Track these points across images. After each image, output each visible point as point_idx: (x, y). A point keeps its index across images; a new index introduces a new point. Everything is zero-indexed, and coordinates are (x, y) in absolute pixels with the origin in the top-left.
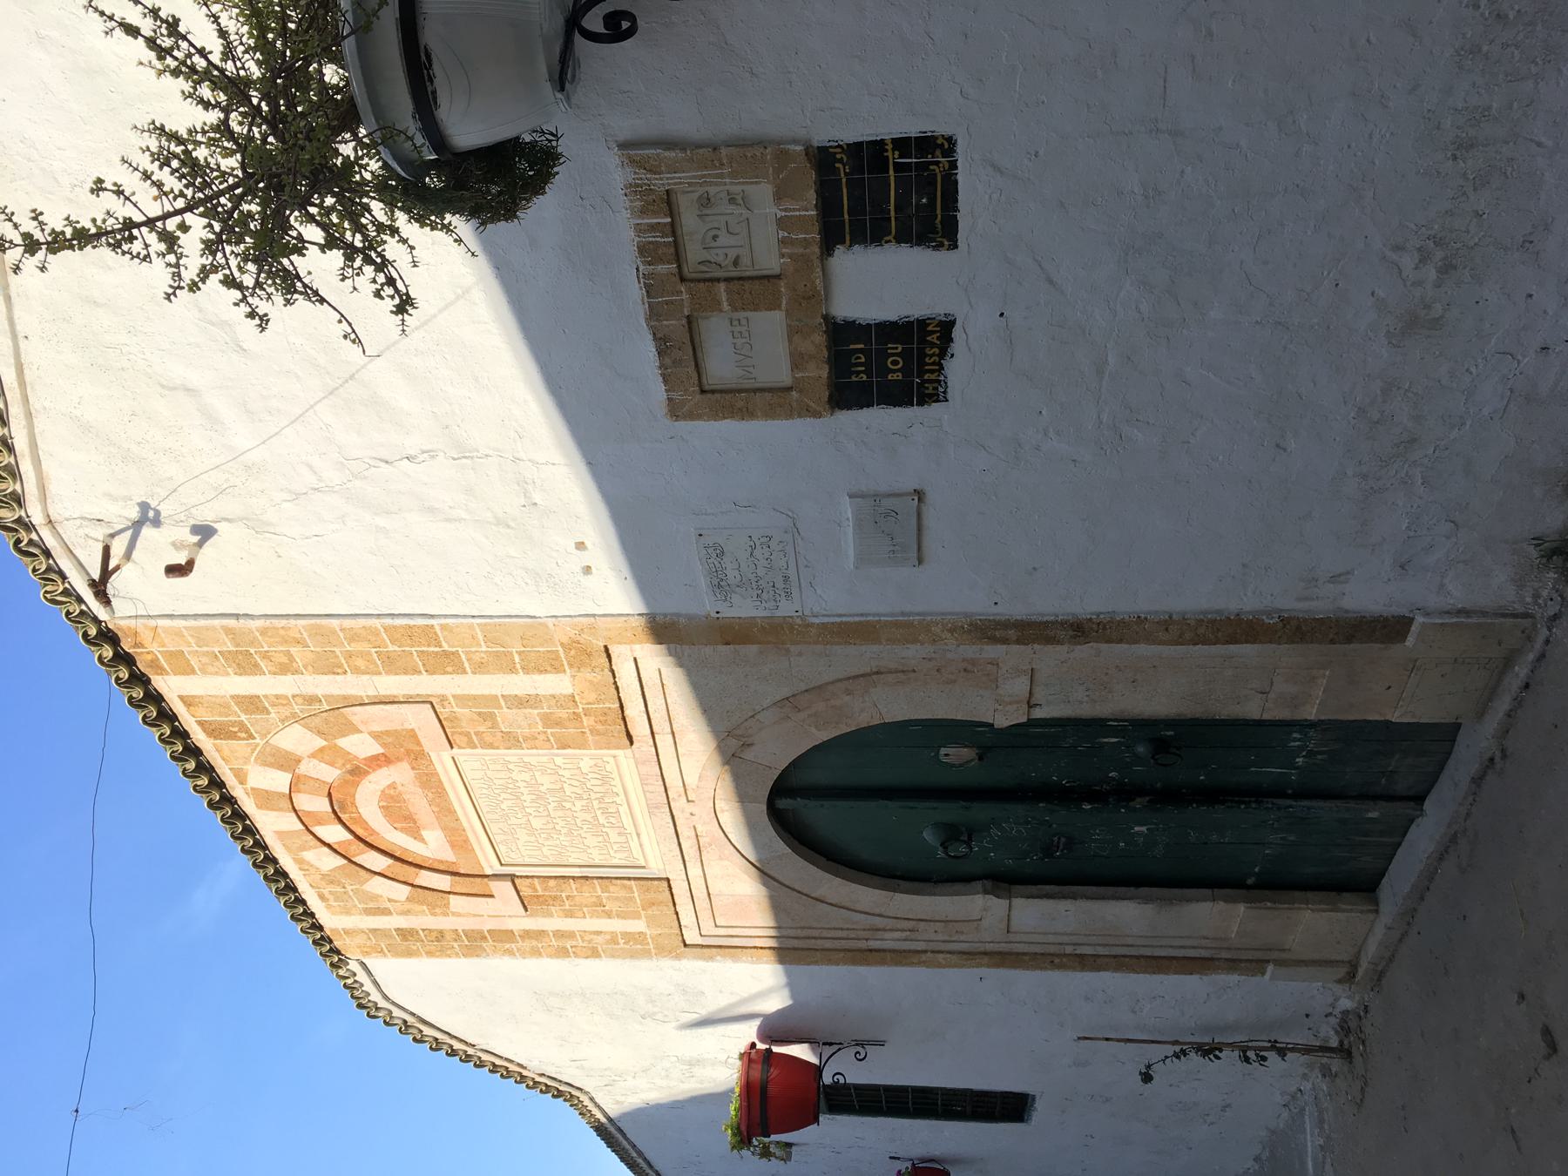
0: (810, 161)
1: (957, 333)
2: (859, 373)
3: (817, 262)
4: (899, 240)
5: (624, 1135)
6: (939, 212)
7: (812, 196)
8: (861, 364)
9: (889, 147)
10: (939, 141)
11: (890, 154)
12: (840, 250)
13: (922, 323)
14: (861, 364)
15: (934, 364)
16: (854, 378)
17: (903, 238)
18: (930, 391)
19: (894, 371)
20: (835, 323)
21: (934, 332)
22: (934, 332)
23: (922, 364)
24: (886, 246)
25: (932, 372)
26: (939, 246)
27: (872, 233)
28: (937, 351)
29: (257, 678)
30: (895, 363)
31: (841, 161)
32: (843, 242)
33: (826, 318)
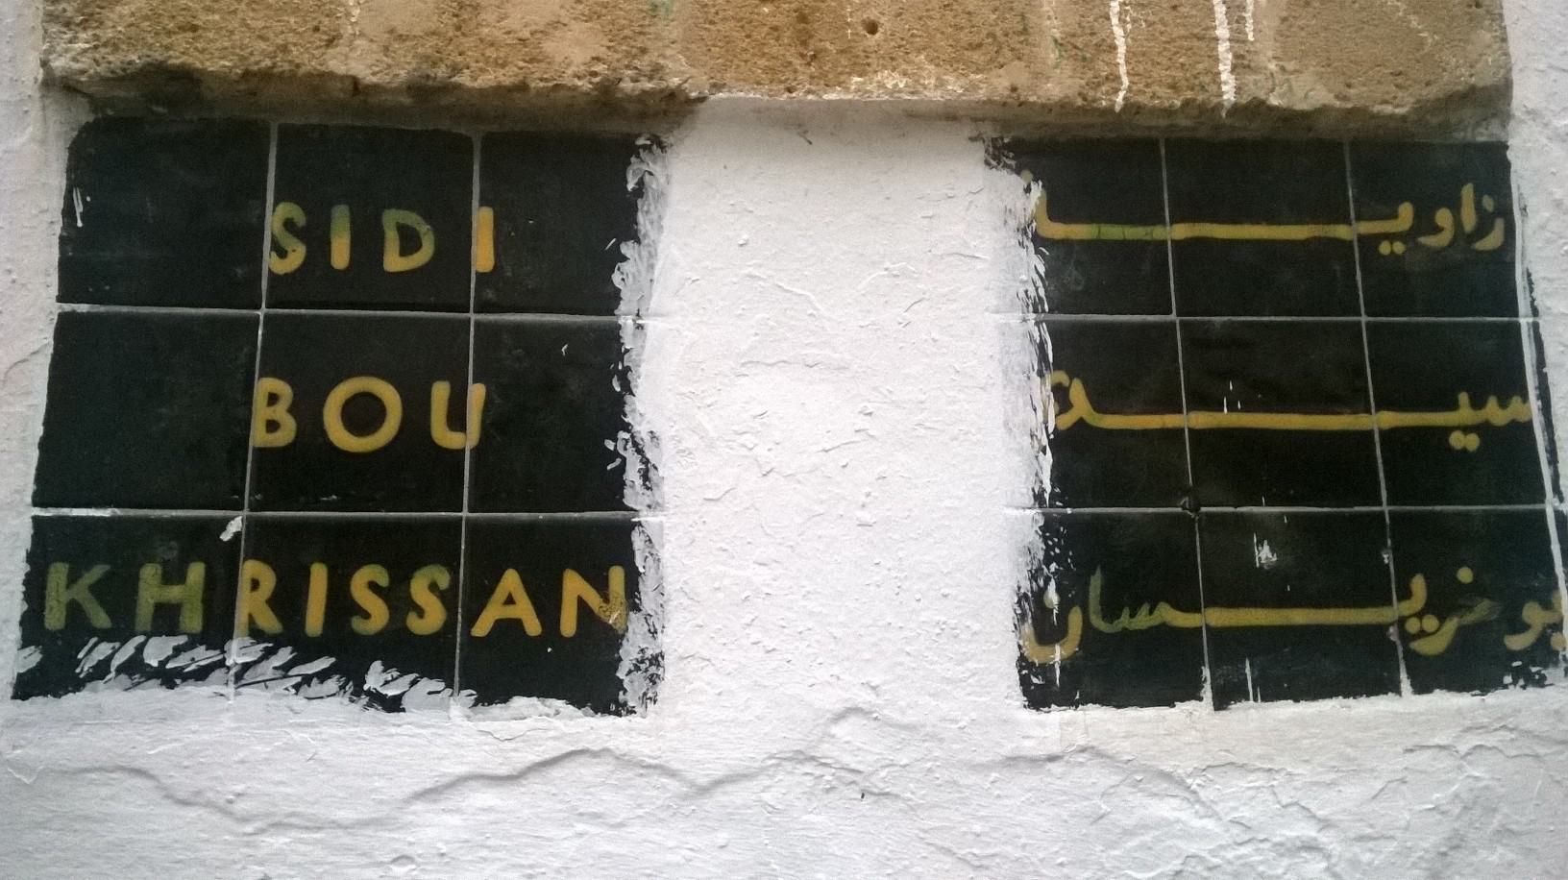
0: (1422, 109)
1: (539, 723)
2: (316, 239)
3: (994, 85)
4: (1071, 448)
5: (1553, 461)
6: (1218, 617)
7: (1305, 91)
8: (368, 244)
9: (1495, 414)
10: (1533, 613)
11: (1465, 414)
12: (1019, 197)
13: (613, 553)
14: (368, 244)
15: (341, 606)
16: (276, 216)
17: (1079, 461)
18: (151, 588)
19: (307, 409)
20: (626, 150)
21: (547, 603)
22: (547, 603)
23: (345, 550)
24: (1041, 391)
25: (288, 601)
26: (1038, 619)
27: (1099, 328)
28: (430, 618)
29: (622, 721)
30: (363, 414)
31: (1425, 223)
32: (1057, 207)
33: (667, 114)
